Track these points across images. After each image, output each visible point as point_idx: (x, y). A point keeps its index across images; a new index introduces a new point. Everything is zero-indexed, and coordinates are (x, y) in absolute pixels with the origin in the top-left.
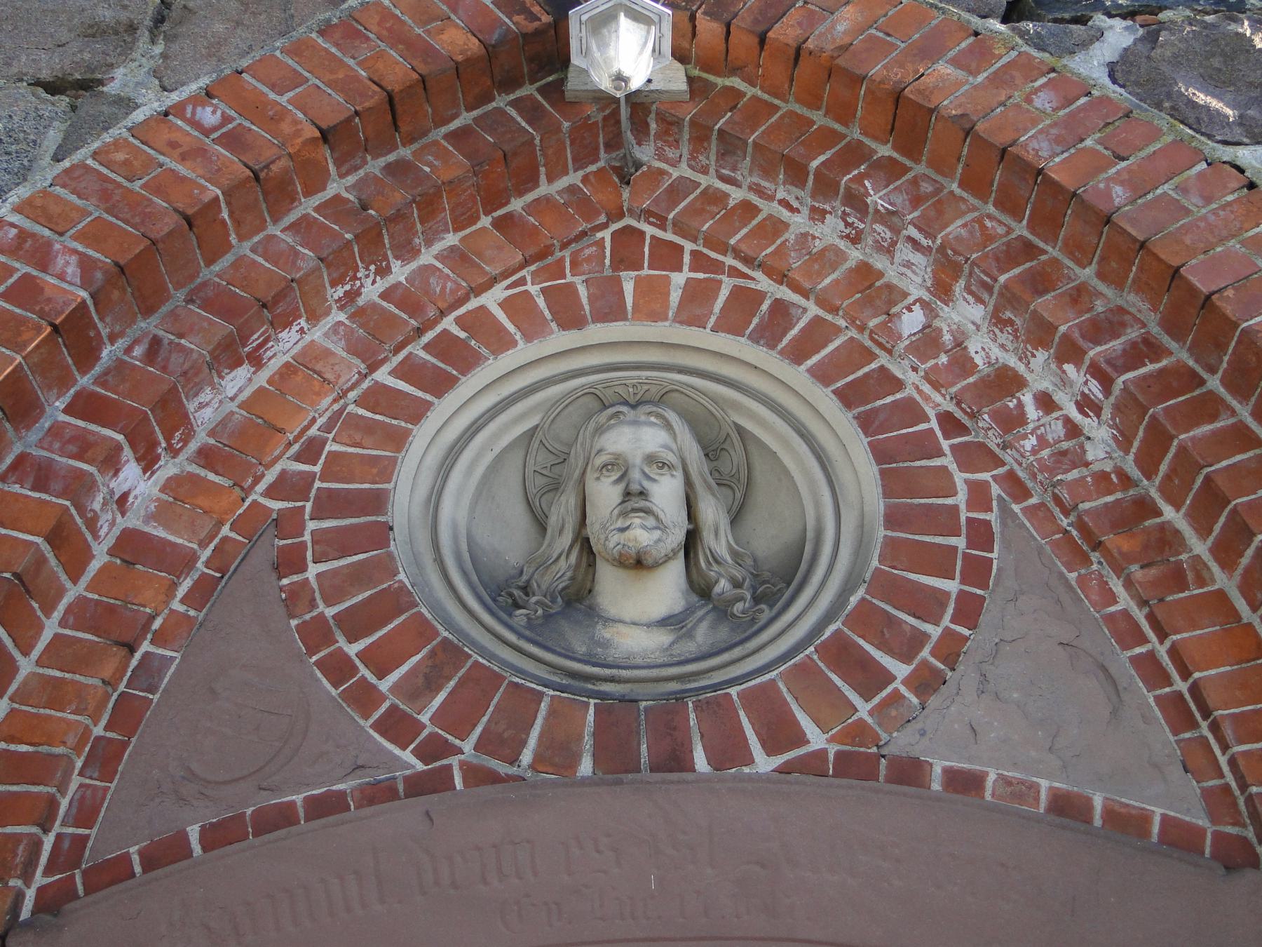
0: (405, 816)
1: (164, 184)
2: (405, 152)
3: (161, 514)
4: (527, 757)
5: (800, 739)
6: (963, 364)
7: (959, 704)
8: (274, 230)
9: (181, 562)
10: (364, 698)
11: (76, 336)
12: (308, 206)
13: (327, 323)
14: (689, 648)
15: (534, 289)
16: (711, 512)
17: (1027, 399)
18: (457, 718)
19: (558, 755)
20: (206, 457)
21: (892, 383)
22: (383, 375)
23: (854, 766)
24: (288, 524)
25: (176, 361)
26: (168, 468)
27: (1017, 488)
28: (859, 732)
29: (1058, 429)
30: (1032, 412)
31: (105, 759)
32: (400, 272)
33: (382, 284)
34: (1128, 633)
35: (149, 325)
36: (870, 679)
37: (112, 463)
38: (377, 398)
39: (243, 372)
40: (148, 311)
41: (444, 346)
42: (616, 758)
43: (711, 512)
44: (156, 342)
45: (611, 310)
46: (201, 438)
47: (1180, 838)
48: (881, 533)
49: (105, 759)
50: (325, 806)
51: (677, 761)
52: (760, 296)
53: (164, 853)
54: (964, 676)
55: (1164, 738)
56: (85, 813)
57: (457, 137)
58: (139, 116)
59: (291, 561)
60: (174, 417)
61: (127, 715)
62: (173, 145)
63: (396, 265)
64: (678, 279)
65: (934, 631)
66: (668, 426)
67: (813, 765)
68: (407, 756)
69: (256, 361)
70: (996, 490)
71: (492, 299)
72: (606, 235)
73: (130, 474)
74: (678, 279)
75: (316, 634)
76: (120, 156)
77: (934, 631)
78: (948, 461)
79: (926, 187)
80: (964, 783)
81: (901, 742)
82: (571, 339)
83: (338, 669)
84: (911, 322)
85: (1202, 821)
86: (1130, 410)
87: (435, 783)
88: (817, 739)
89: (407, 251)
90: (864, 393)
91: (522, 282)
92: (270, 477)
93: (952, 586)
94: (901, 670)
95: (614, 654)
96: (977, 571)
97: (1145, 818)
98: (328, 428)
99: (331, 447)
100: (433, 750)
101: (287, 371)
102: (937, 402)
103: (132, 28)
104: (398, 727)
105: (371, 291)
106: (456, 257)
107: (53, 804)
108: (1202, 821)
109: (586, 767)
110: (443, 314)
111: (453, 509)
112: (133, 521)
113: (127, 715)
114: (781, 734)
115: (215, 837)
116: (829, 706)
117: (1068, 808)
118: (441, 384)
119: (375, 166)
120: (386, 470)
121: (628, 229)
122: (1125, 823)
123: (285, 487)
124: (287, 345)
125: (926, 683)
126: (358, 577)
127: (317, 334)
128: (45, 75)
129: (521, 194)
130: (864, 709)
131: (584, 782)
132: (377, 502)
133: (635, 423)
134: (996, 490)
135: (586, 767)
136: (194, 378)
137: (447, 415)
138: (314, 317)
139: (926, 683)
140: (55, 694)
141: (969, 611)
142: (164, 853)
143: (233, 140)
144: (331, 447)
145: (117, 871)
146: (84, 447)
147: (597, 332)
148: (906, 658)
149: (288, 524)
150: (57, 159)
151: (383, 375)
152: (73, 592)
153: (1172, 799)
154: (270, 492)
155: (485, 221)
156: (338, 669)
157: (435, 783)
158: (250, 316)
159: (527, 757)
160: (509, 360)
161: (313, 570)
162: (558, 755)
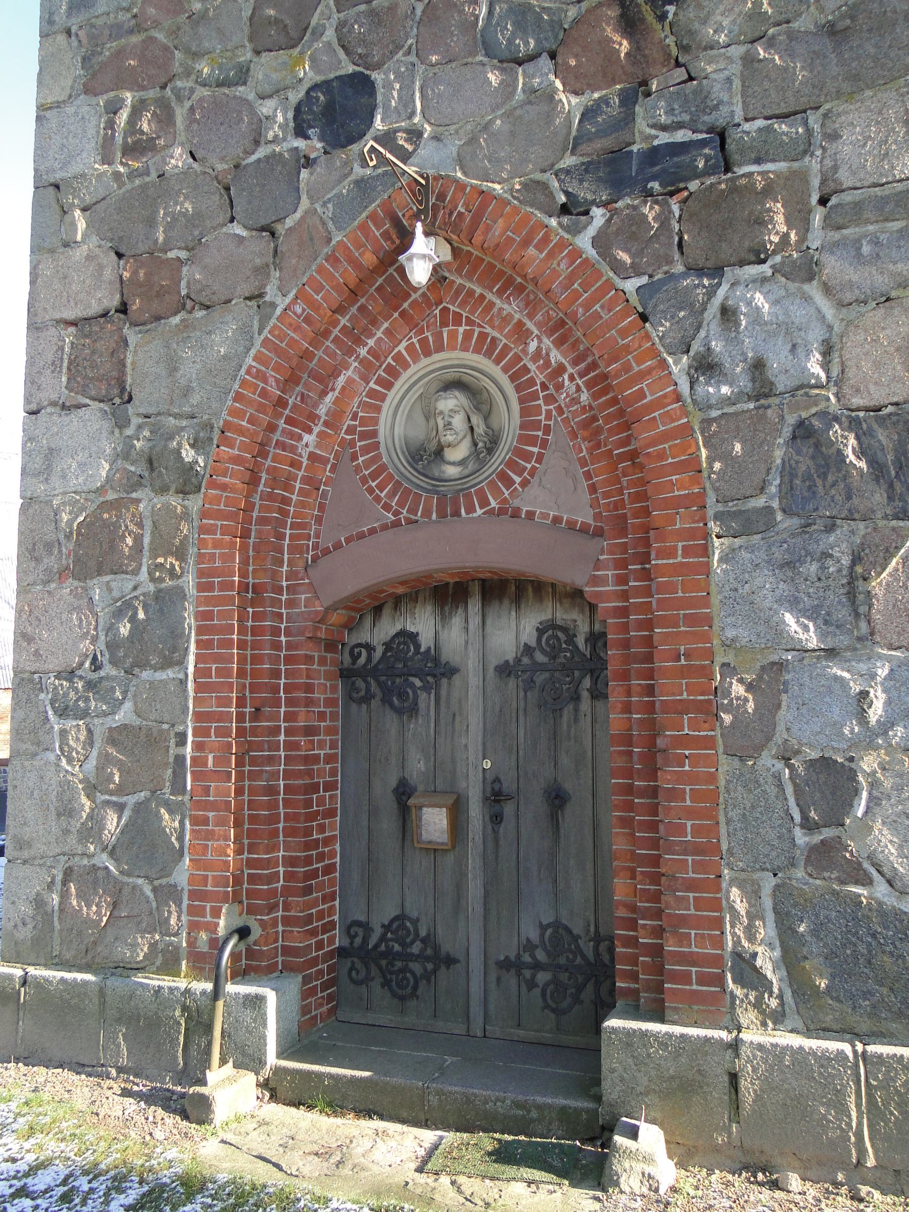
0: (389, 534)
1: (292, 343)
2: (363, 300)
3: (318, 445)
4: (419, 514)
5: (489, 504)
6: (548, 363)
7: (533, 490)
8: (328, 343)
9: (325, 461)
10: (378, 499)
11: (281, 403)
12: (336, 332)
13: (352, 368)
14: (467, 472)
15: (415, 340)
16: (476, 420)
17: (566, 376)
18: (401, 504)
19: (427, 513)
20: (326, 424)
21: (526, 370)
22: (372, 385)
23: (502, 511)
24: (352, 444)
25: (309, 401)
26: (316, 430)
27: (560, 411)
28: (505, 501)
29: (574, 388)
30: (567, 383)
31: (319, 520)
32: (371, 342)
33: (366, 349)
34: (583, 463)
35: (299, 389)
36: (509, 483)
37: (300, 438)
38: (372, 394)
39: (330, 394)
40: (298, 385)
41: (390, 370)
42: (442, 514)
43: (476, 420)
44: (303, 394)
45: (440, 348)
46: (323, 418)
47: (584, 529)
48: (518, 432)
49: (319, 520)
50: (372, 531)
51: (457, 513)
52: (487, 334)
53: (338, 546)
54: (535, 481)
55: (586, 497)
56: (317, 536)
57: (380, 289)
58: (278, 311)
59: (354, 457)
60: (313, 417)
61: (322, 508)
62: (291, 325)
63: (369, 341)
64: (461, 330)
65: (529, 466)
66: (456, 397)
67: (491, 512)
68: (390, 515)
69: (333, 389)
70: (554, 412)
71: (401, 347)
72: (437, 311)
73: (307, 438)
74: (461, 330)
75: (364, 480)
76: (277, 333)
77: (529, 466)
78: (541, 402)
79: (532, 297)
80: (530, 515)
81: (516, 503)
82: (428, 360)
83: (371, 491)
84: (533, 346)
85: (592, 522)
86: (589, 385)
87: (396, 524)
88: (493, 504)
89: (371, 335)
90: (518, 375)
91: (411, 338)
92: (345, 428)
93: (535, 450)
94: (518, 480)
95: (446, 476)
96: (544, 444)
97: (577, 522)
98: (358, 407)
99: (360, 414)
100: (396, 513)
101: (343, 388)
102: (540, 378)
103: (268, 265)
104: (387, 507)
105: (363, 352)
106: (388, 332)
107: (309, 535)
108: (592, 522)
109: (434, 516)
110: (386, 358)
111: (398, 431)
112: (311, 449)
113: (322, 508)
114: (484, 503)
115: (348, 540)
116: (497, 492)
117: (557, 520)
118: (388, 386)
119: (354, 310)
120: (376, 421)
121: (445, 308)
122: (571, 525)
123: (351, 430)
124: (341, 381)
125: (525, 484)
126: (373, 460)
127: (349, 373)
128: (247, 295)
129: (405, 301)
130: (506, 493)
131: (435, 522)
132: (374, 434)
133: (446, 398)
134: (554, 412)
135: (434, 516)
136: (316, 405)
137: (393, 396)
138: (347, 369)
139: (525, 484)
140: (302, 504)
141: (540, 459)
142: (338, 546)
143: (307, 320)
144: (360, 414)
145: (326, 552)
146: (292, 436)
147: (436, 357)
148: (520, 476)
149: (352, 444)
150: (259, 334)
151: (372, 385)
152: (300, 474)
153: (585, 516)
154: (346, 433)
155: (396, 315)
156: (371, 491)
157: (396, 524)
158: (325, 379)
159: (419, 514)
160: (410, 372)
161: (361, 459)
162: (427, 513)
